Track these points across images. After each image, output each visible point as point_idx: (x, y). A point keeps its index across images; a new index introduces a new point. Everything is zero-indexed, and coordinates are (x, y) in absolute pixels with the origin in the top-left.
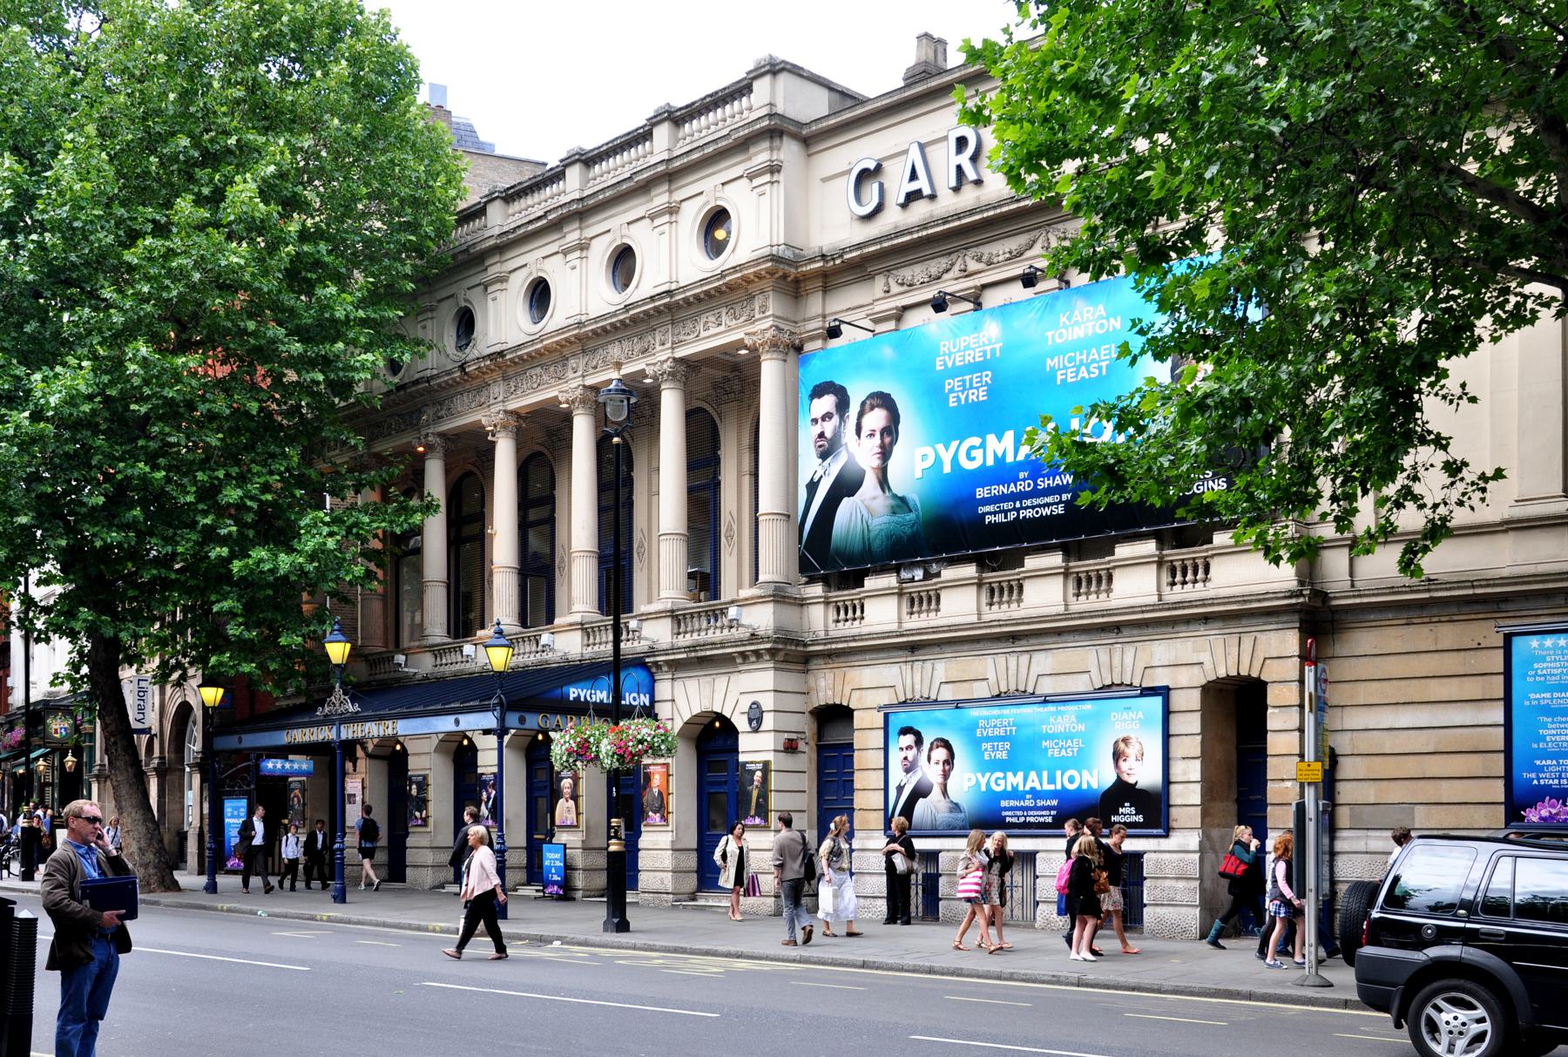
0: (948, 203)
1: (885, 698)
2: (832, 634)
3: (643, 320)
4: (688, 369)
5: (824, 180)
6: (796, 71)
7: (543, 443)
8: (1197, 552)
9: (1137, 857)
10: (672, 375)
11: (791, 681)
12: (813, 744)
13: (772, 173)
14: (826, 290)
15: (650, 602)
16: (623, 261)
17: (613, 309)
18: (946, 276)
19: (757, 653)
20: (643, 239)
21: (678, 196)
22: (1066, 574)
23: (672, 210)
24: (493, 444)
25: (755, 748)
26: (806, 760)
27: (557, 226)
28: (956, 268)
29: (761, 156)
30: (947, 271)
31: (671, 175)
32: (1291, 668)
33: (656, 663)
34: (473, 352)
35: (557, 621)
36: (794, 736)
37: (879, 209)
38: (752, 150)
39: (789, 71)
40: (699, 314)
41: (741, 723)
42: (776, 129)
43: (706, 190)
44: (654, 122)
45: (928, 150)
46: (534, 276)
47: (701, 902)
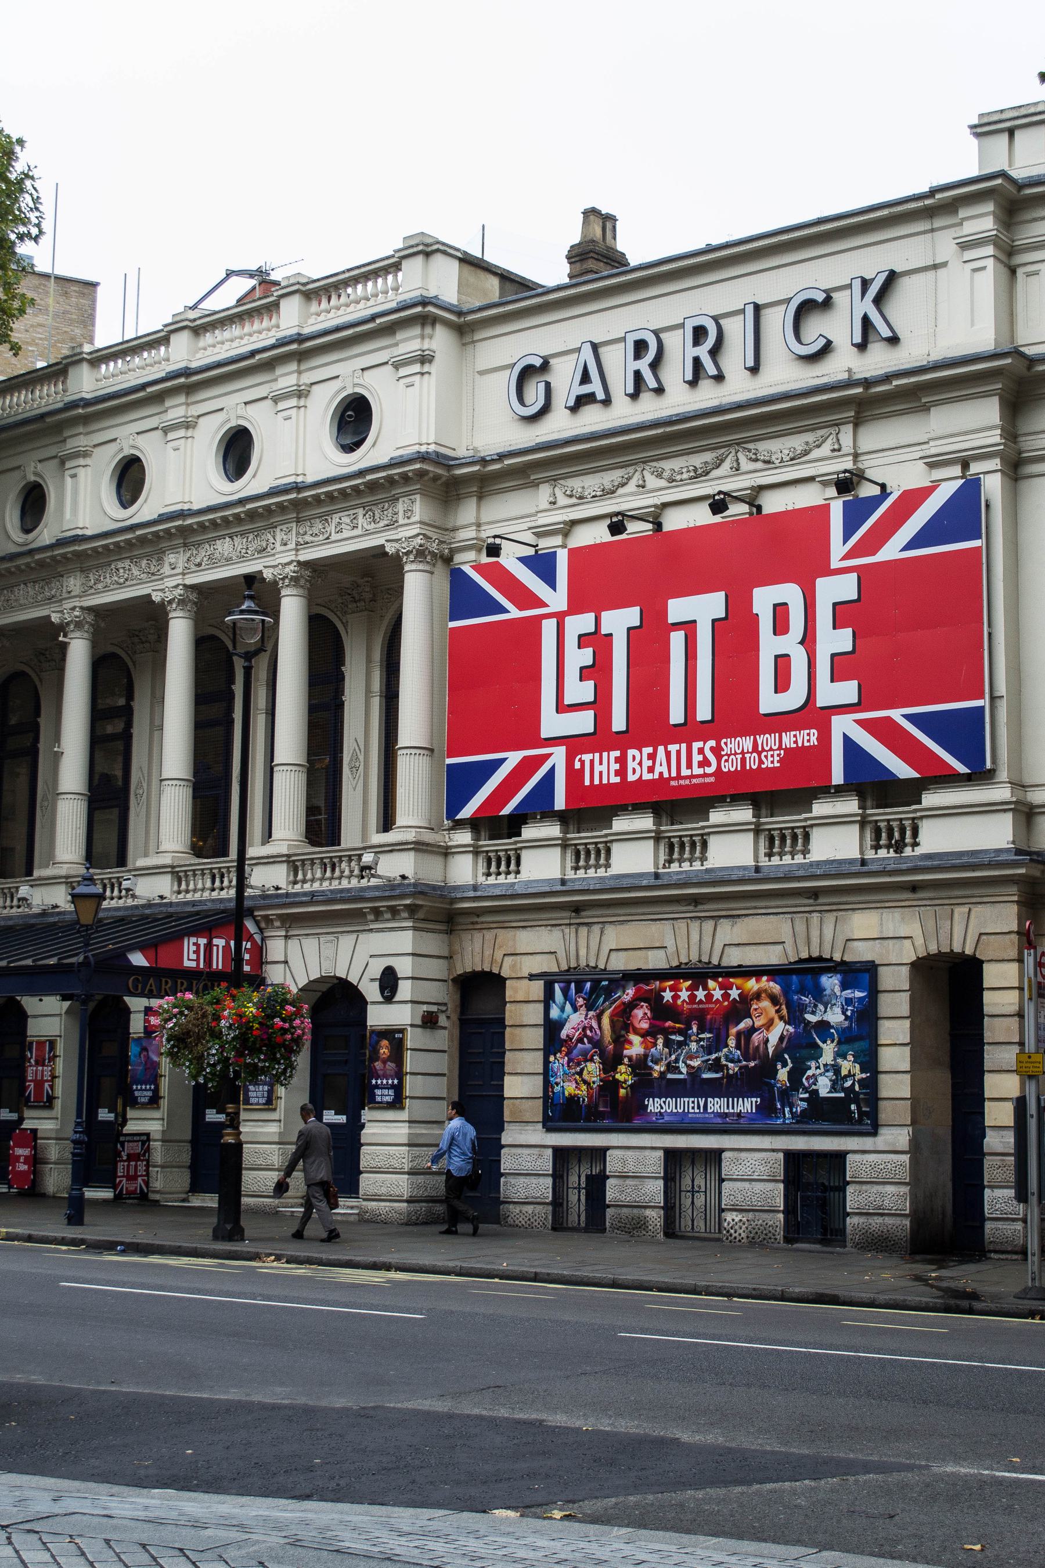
1: (549, 966)
3: (151, 541)
4: (316, 575)
5: (481, 373)
7: (127, 646)
8: (598, 835)
9: (839, 1158)
10: (295, 581)
11: (433, 943)
12: (455, 1017)
13: (423, 363)
15: (146, 855)
16: (237, 450)
18: (621, 491)
20: (262, 422)
21: (307, 378)
22: (564, 846)
23: (301, 393)
24: (64, 647)
26: (443, 1038)
28: (633, 482)
29: (409, 342)
30: (623, 485)
31: (301, 350)
32: (1010, 946)
33: (266, 918)
34: (46, 534)
35: (37, 873)
36: (434, 1008)
38: (400, 336)
39: (444, 253)
40: (330, 513)
41: (371, 991)
42: (422, 314)
43: (128, 435)
45: (763, 312)
46: (233, 423)
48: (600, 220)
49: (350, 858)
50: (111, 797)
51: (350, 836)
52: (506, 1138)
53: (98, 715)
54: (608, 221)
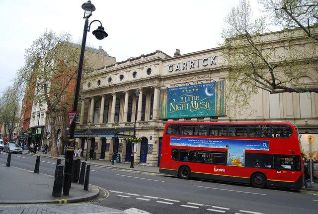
0: (182, 71)
6: (162, 52)
11: (156, 133)
16: (122, 77)
17: (279, 60)
23: (143, 68)
26: (157, 145)
29: (156, 62)
31: (130, 67)
41: (149, 139)
42: (159, 59)
43: (110, 75)
44: (128, 60)
50: (117, 114)
51: (146, 120)
52: (147, 156)
53: (105, 106)
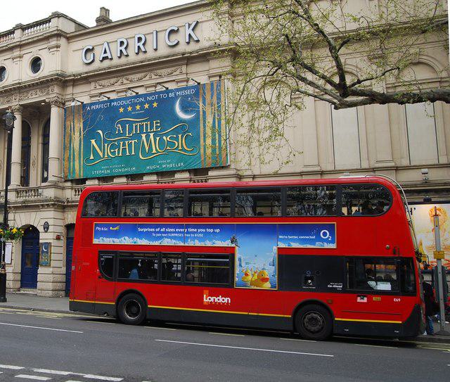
0: (116, 61)
2: (73, 199)
4: (25, 109)
11: (59, 215)
14: (73, 86)
16: (36, 64)
19: (48, 205)
25: (44, 237)
26: (63, 243)
27: (11, 49)
29: (53, 42)
37: (93, 61)
38: (50, 40)
41: (41, 229)
42: (59, 34)
43: (34, 51)
47: (22, 292)
48: (105, 11)
49: (31, 190)
54: (107, 11)
